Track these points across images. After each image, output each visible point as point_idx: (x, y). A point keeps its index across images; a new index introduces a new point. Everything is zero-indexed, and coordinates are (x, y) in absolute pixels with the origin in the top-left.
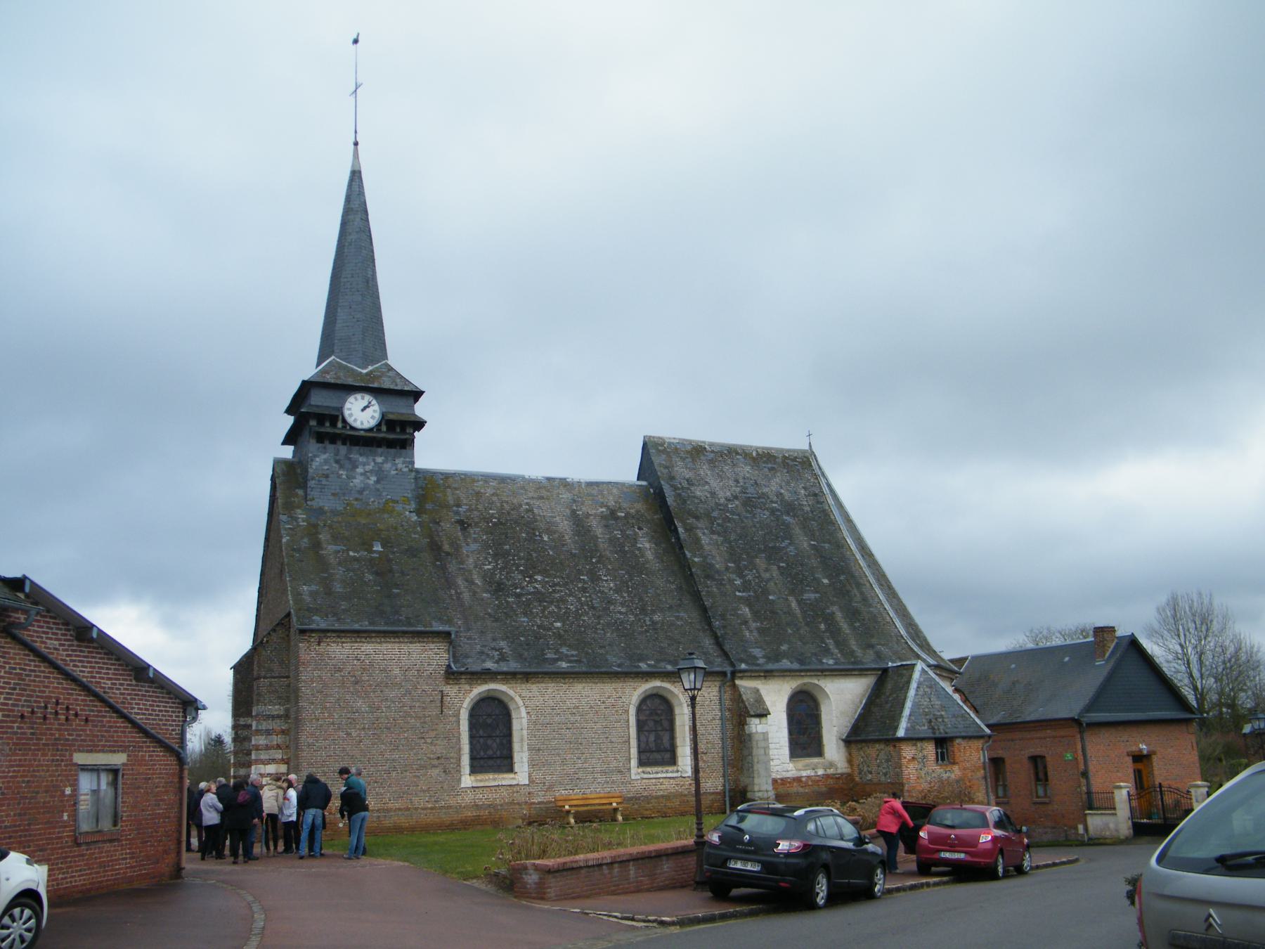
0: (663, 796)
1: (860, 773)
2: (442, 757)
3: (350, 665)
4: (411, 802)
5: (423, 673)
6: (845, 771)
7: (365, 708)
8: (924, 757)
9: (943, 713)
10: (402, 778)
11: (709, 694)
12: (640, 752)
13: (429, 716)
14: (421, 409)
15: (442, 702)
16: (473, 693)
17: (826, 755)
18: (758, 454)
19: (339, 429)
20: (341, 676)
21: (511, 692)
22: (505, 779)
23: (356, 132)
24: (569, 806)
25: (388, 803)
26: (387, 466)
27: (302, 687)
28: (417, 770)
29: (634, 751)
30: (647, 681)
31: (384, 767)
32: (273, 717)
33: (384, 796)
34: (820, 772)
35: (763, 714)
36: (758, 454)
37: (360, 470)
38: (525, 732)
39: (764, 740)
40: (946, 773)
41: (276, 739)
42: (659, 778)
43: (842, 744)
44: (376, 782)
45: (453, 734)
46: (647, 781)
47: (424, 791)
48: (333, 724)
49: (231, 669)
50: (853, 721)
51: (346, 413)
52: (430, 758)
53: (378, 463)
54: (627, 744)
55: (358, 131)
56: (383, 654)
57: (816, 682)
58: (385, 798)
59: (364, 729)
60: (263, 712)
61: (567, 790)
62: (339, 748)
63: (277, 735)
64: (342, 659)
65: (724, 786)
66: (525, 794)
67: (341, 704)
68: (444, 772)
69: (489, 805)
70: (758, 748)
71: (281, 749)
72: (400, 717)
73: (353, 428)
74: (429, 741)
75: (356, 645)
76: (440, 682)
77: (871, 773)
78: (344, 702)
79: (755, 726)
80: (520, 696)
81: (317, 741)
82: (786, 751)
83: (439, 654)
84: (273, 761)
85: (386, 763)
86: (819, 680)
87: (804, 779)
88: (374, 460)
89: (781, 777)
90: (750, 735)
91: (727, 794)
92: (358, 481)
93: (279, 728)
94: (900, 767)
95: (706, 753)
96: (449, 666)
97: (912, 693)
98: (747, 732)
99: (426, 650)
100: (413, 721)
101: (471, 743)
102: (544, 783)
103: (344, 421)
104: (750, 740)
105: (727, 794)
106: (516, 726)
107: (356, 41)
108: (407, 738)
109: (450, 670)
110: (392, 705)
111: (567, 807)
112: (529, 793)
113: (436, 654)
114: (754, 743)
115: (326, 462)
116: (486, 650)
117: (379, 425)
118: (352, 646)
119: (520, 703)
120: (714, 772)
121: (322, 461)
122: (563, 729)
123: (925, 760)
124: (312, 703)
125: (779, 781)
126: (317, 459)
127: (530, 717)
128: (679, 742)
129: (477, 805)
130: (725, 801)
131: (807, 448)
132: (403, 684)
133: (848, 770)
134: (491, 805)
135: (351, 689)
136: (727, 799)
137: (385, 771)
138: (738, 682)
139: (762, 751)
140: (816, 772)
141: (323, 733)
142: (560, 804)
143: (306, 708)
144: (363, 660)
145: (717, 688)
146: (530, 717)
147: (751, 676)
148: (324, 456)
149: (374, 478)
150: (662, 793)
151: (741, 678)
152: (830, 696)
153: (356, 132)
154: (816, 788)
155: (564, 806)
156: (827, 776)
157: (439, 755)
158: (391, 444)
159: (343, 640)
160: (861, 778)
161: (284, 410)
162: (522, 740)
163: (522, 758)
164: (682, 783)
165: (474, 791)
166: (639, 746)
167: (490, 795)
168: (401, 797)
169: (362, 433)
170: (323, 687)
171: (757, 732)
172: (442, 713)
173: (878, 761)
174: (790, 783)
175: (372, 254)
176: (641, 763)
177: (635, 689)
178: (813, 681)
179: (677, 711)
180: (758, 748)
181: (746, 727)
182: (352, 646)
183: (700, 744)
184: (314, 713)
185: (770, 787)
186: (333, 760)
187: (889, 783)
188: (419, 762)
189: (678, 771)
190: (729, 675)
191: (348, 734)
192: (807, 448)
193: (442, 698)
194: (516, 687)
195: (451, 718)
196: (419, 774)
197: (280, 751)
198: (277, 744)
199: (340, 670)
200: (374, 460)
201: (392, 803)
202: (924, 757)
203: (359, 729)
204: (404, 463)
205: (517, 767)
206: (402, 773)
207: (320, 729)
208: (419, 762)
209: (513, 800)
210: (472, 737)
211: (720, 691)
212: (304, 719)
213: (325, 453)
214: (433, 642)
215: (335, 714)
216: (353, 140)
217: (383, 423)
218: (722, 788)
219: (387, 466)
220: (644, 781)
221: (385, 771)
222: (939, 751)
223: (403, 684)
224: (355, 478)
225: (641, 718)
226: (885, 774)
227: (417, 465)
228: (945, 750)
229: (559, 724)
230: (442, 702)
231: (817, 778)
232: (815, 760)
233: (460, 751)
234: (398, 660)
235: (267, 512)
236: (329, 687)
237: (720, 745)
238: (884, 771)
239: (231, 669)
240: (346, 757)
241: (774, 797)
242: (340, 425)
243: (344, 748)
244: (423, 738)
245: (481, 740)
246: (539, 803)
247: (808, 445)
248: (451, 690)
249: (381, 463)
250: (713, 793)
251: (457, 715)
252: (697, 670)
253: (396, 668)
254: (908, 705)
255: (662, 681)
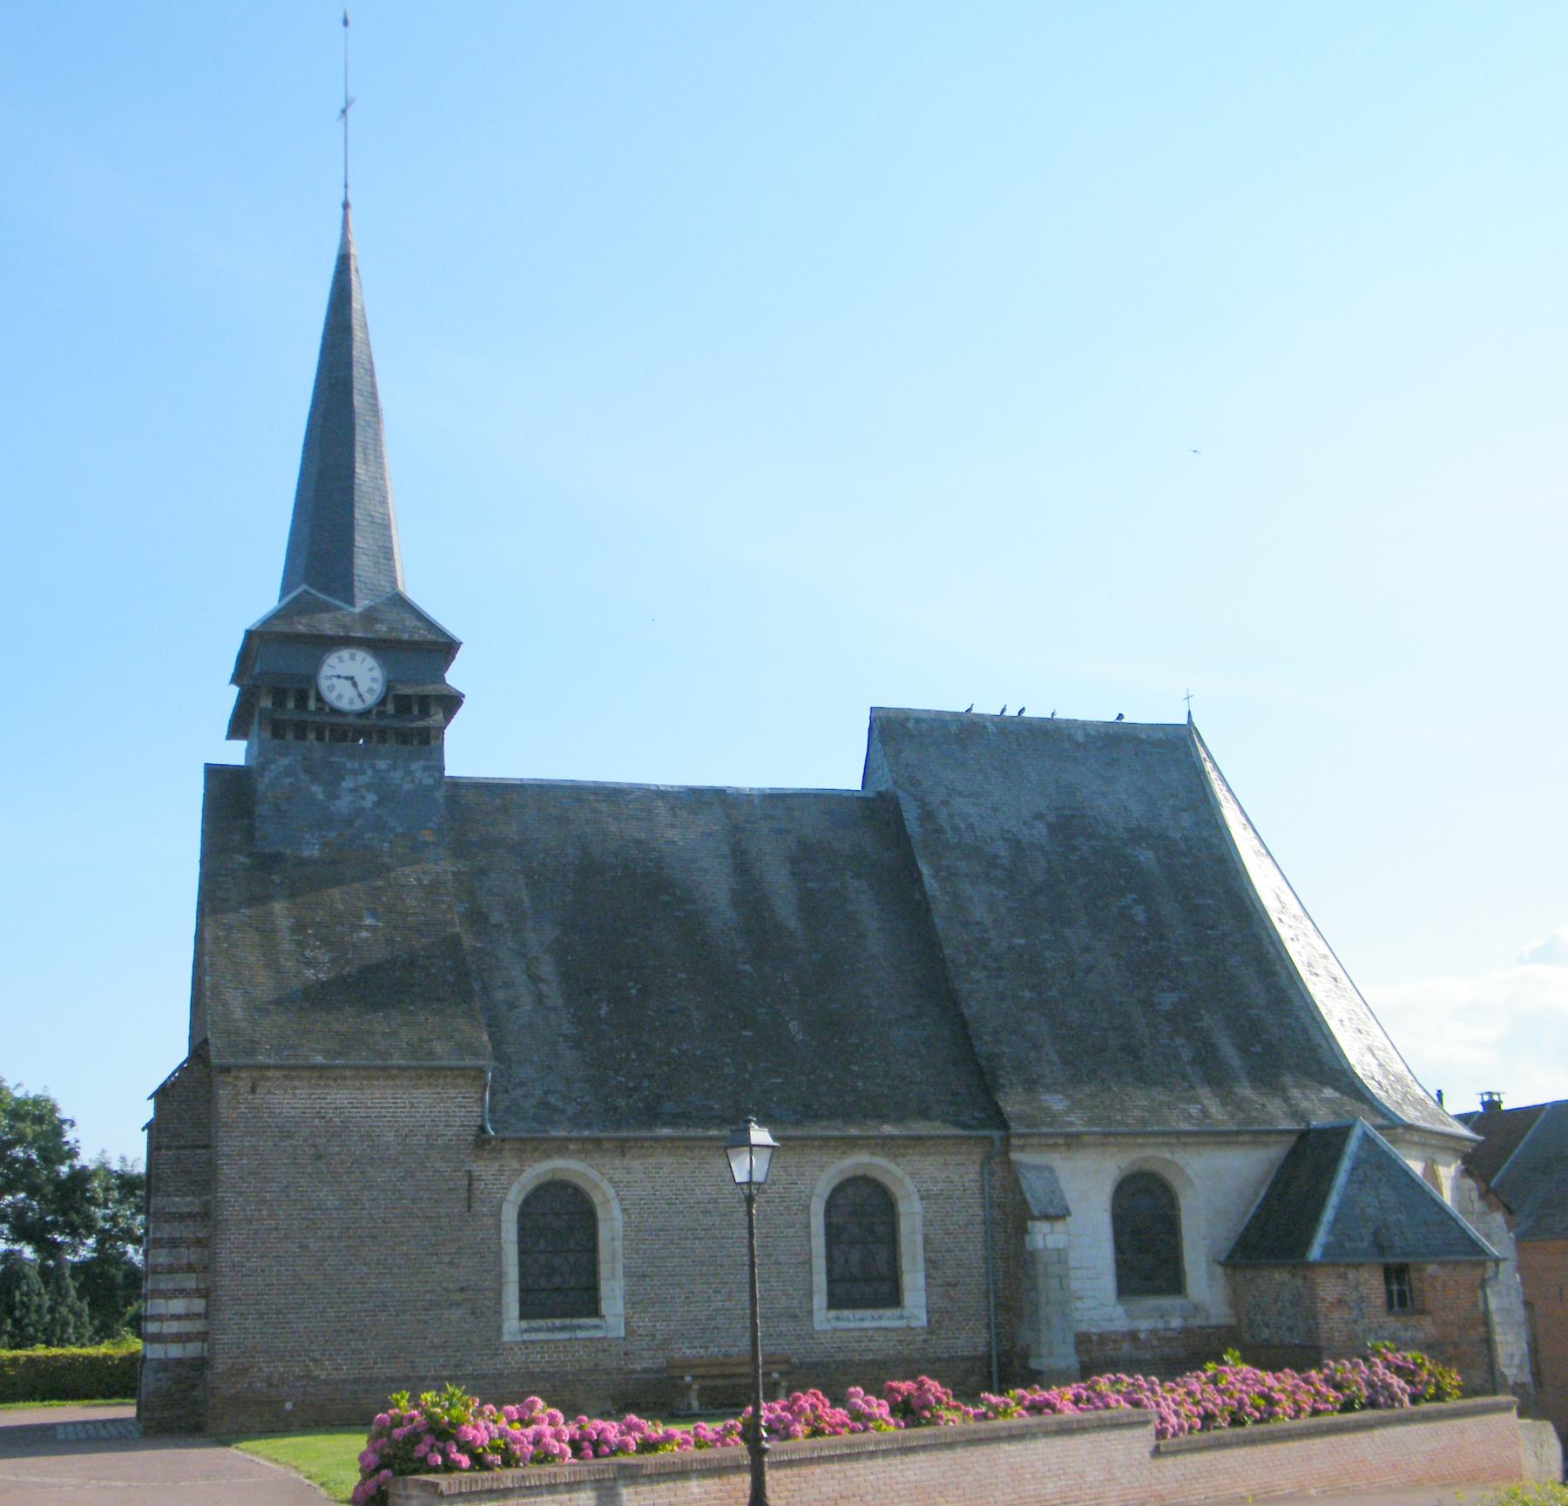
0: (873, 1362)
1: (1251, 1325)
2: (469, 1286)
3: (306, 1127)
4: (414, 1367)
5: (437, 1140)
6: (1224, 1321)
7: (332, 1201)
8: (1362, 1299)
9: (1402, 1217)
10: (397, 1324)
11: (961, 1177)
12: (831, 1281)
13: (448, 1215)
14: (456, 676)
15: (469, 1190)
16: (525, 1174)
17: (1188, 1290)
18: (1087, 735)
19: (311, 712)
20: (291, 1146)
21: (594, 1174)
22: (586, 1330)
23: (346, 186)
24: (692, 1376)
25: (372, 1368)
26: (397, 776)
27: (223, 1164)
28: (425, 1309)
29: (820, 1280)
30: (844, 1153)
31: (366, 1305)
32: (182, 1217)
33: (364, 1356)
34: (1176, 1323)
35: (1058, 1214)
36: (1087, 735)
37: (348, 784)
38: (618, 1244)
39: (1059, 1262)
40: (1406, 1330)
41: (189, 1255)
42: (867, 1329)
43: (1219, 1270)
44: (352, 1331)
45: (489, 1248)
46: (844, 1334)
47: (436, 1347)
48: (276, 1229)
49: (143, 1129)
50: (1240, 1229)
51: (324, 684)
52: (447, 1290)
53: (380, 771)
54: (807, 1266)
55: (349, 183)
56: (366, 1108)
57: (1168, 1155)
58: (366, 1359)
59: (330, 1237)
60: (163, 1208)
61: (695, 1347)
62: (287, 1270)
63: (188, 1248)
64: (293, 1117)
65: (989, 1344)
66: (618, 1355)
67: (291, 1194)
68: (472, 1313)
69: (554, 1374)
70: (1047, 1276)
71: (195, 1272)
72: (396, 1216)
73: (336, 711)
74: (446, 1259)
75: (319, 1091)
76: (468, 1155)
77: (1267, 1326)
78: (296, 1191)
79: (1044, 1236)
80: (611, 1180)
81: (248, 1260)
82: (1109, 1282)
83: (464, 1107)
84: (180, 1292)
85: (370, 1297)
86: (1173, 1153)
87: (1142, 1336)
88: (373, 766)
89: (1099, 1331)
90: (1033, 1253)
91: (994, 1358)
92: (344, 804)
93: (191, 1236)
94: (1315, 1318)
95: (955, 1285)
96: (482, 1129)
97: (1341, 1178)
98: (1029, 1247)
99: (442, 1099)
100: (419, 1224)
101: (522, 1264)
102: (654, 1335)
103: (319, 698)
104: (1033, 1262)
105: (994, 1358)
106: (603, 1234)
107: (346, 23)
108: (407, 1254)
109: (484, 1136)
110: (382, 1196)
111: (688, 1379)
112: (626, 1354)
113: (459, 1107)
114: (1040, 1268)
115: (288, 771)
116: (552, 1099)
117: (382, 702)
118: (311, 1094)
119: (611, 1192)
120: (970, 1320)
121: (282, 769)
122: (687, 1239)
123: (1364, 1305)
124: (240, 1193)
125: (1094, 1338)
126: (273, 767)
127: (630, 1217)
128: (905, 1263)
129: (532, 1373)
130: (990, 1373)
131: (1185, 721)
132: (401, 1160)
133: (1233, 1321)
134: (557, 1372)
135: (309, 1169)
136: (994, 1369)
137: (365, 1311)
138: (1015, 1156)
139: (1055, 1284)
140: (1167, 1323)
141: (259, 1245)
142: (676, 1373)
143: (229, 1201)
144: (331, 1118)
145: (977, 1168)
146: (630, 1217)
147: (1039, 1145)
148: (286, 761)
149: (371, 798)
150: (871, 1356)
151: (1022, 1148)
152: (1196, 1182)
153: (346, 186)
154: (1167, 1350)
155: (682, 1378)
156: (1186, 1331)
157: (464, 1284)
158: (404, 738)
159: (296, 1083)
160: (1253, 1337)
161: (229, 680)
162: (613, 1259)
163: (613, 1291)
164: (909, 1338)
165: (526, 1348)
166: (829, 1272)
167: (555, 1355)
168: (395, 1357)
169: (351, 719)
170: (259, 1164)
171: (1046, 1248)
172: (469, 1211)
173: (1279, 1304)
174: (1115, 1341)
175: (373, 402)
176: (835, 1302)
177: (822, 1168)
178: (1160, 1155)
179: (902, 1207)
180: (1047, 1276)
181: (1028, 1238)
182: (311, 1094)
183: (748, 1272)
184: (244, 1210)
185: (1071, 1350)
186: (274, 1292)
187: (1296, 1346)
188: (428, 1296)
189: (901, 1317)
190: (997, 1143)
191: (303, 1247)
192: (1185, 721)
193: (470, 1185)
194: (603, 1165)
195: (485, 1219)
196: (428, 1317)
197: (194, 1275)
198: (189, 1264)
199: (290, 1136)
200: (373, 766)
201: (379, 1368)
202: (1362, 1299)
203: (322, 1238)
204: (426, 769)
205: (604, 1307)
206: (397, 1315)
207: (253, 1239)
208: (428, 1296)
209: (596, 1365)
210: (523, 1252)
211: (982, 1173)
212: (227, 1220)
213: (287, 755)
214: (455, 1086)
215: (281, 1213)
216: (342, 199)
217: (390, 699)
218: (986, 1349)
219: (397, 776)
220: (838, 1334)
221: (365, 1311)
222: (1395, 1287)
223: (401, 1160)
224: (337, 797)
225: (835, 1220)
226: (1291, 1329)
227: (447, 773)
228: (1406, 1288)
229: (682, 1230)
230: (469, 1190)
231: (1169, 1334)
232: (1166, 1302)
233: (501, 1277)
234: (393, 1117)
235: (199, 858)
236: (269, 1164)
237: (982, 1271)
238: (1289, 1323)
239: (143, 1129)
240: (299, 1287)
241: (1078, 1366)
242: (312, 705)
243: (295, 1271)
244: (437, 1254)
245: (542, 1258)
246: (645, 1371)
247: (1187, 716)
248: (485, 1169)
249: (385, 771)
250: (968, 1359)
251: (496, 1214)
252: (754, 1149)
253: (389, 1132)
254: (1333, 1200)
255: (873, 1154)
